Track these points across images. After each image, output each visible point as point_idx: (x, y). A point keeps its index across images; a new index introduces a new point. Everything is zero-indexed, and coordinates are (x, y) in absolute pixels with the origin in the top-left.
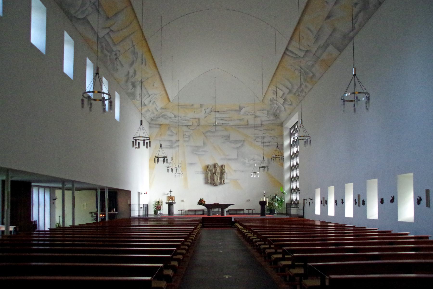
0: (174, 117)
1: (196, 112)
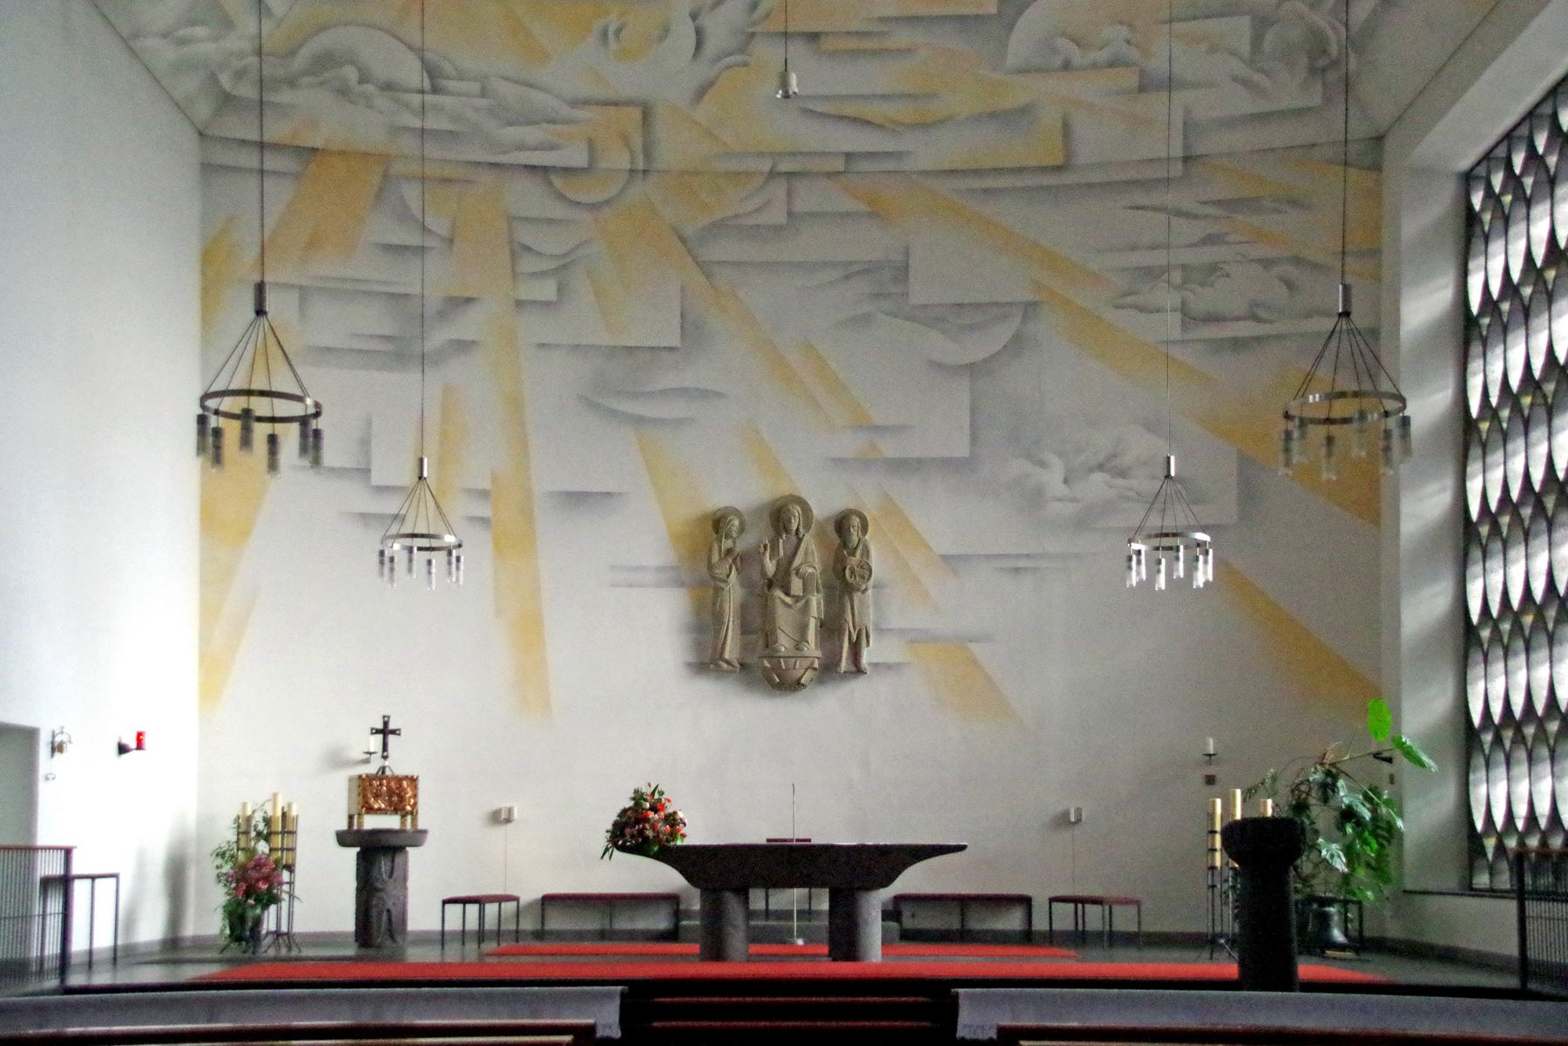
0: (427, 84)
1: (619, 31)
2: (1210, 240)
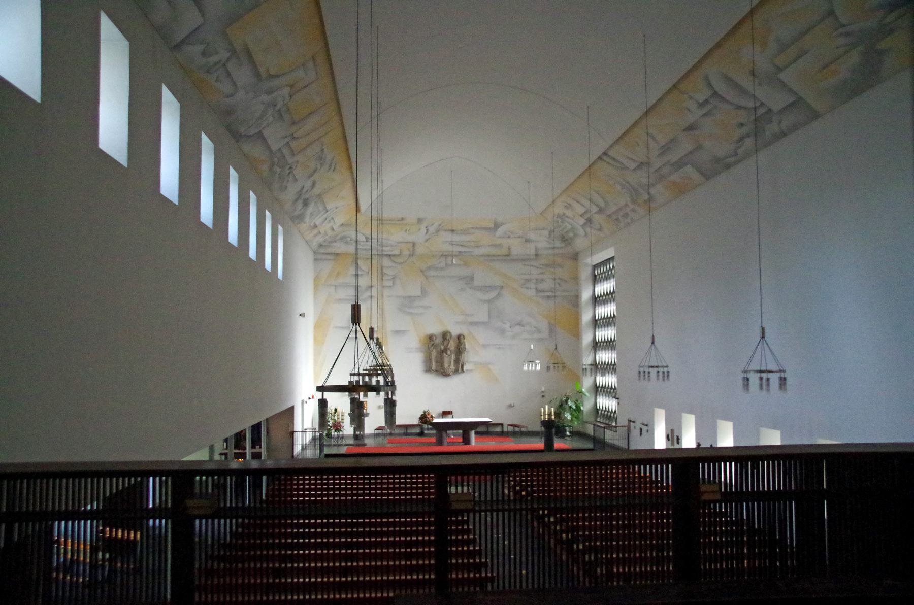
2: (542, 273)
